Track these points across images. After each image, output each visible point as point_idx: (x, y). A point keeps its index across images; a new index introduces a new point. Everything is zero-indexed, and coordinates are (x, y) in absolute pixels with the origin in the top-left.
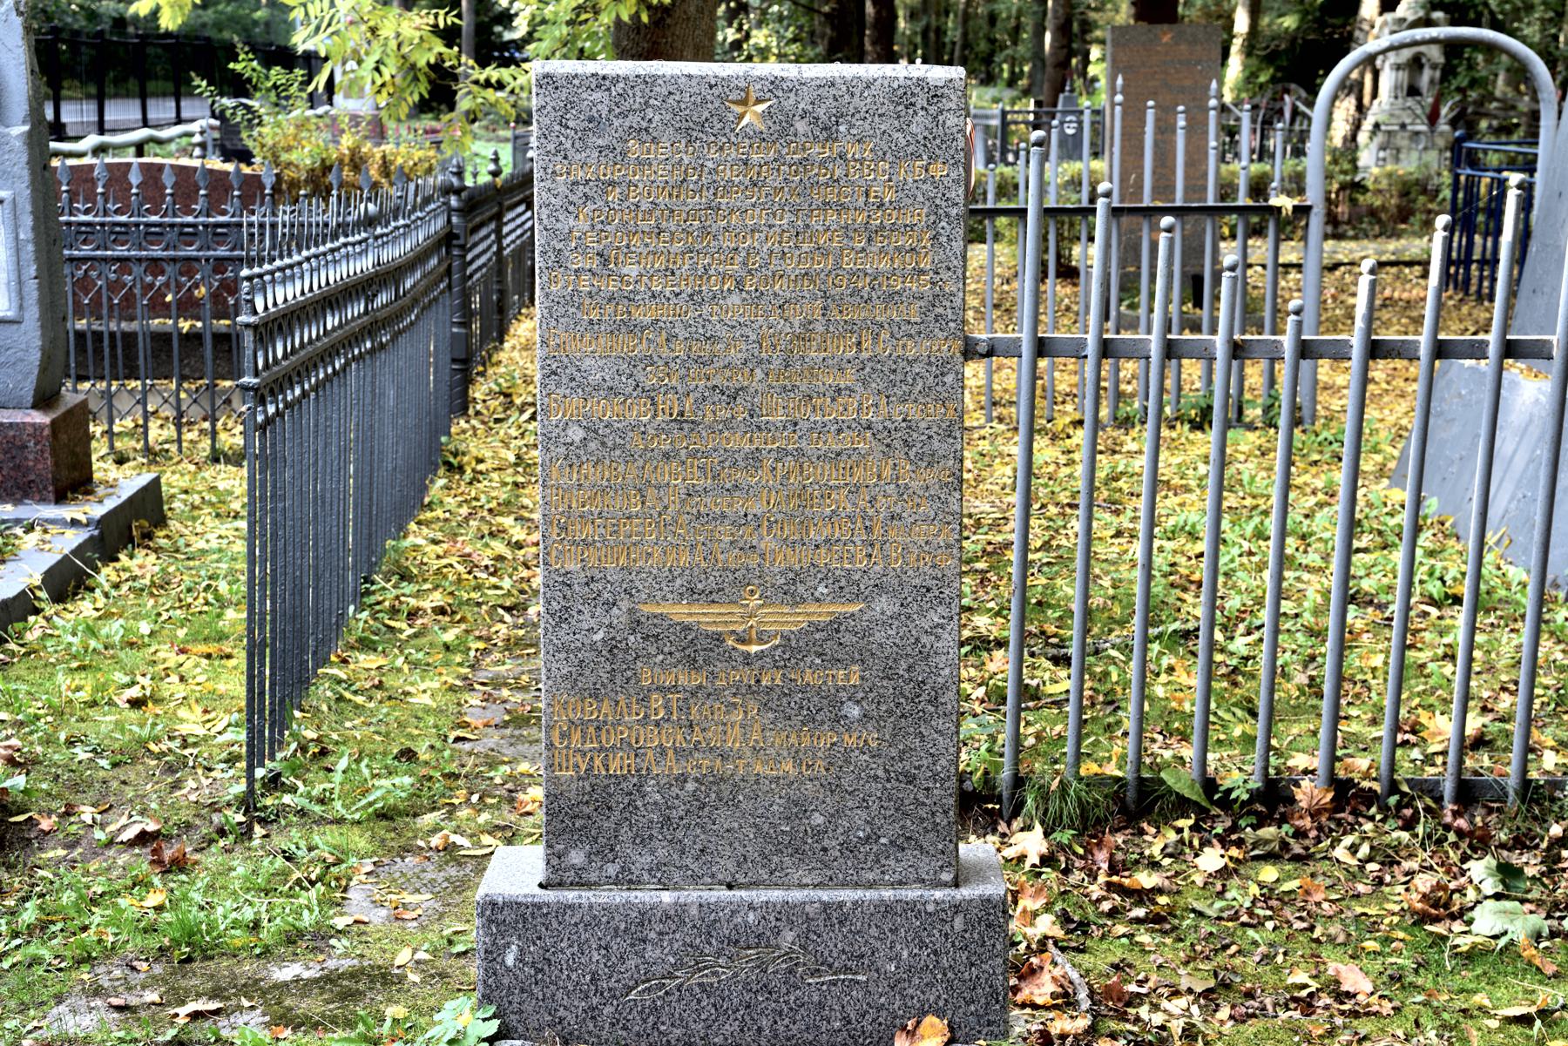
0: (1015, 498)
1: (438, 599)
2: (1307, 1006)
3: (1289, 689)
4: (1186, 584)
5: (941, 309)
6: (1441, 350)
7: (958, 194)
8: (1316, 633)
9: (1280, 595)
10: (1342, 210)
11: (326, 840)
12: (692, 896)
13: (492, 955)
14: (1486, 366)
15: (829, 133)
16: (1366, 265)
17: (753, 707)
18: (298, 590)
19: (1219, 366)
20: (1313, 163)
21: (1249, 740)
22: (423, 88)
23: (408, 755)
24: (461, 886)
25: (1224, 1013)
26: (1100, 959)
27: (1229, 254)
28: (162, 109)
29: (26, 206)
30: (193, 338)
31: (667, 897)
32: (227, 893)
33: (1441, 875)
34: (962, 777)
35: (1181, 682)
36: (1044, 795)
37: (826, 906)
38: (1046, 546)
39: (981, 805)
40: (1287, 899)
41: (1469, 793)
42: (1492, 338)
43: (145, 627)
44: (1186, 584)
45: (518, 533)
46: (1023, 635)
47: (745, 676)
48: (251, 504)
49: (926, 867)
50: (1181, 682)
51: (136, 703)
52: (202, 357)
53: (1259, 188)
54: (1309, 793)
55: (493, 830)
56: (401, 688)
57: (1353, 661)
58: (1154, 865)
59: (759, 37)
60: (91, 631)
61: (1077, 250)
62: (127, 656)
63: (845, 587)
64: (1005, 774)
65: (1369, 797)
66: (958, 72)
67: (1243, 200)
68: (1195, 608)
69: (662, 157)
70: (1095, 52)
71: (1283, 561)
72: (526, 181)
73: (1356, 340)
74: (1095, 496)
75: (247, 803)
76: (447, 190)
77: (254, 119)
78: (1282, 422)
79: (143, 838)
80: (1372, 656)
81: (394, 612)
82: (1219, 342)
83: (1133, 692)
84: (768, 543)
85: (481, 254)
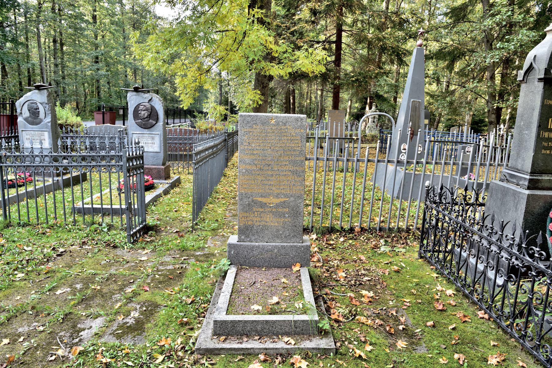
0: (313, 182)
1: (222, 196)
2: (356, 262)
3: (354, 213)
4: (340, 196)
5: (302, 152)
6: (378, 161)
7: (305, 135)
8: (358, 204)
9: (353, 198)
10: (364, 139)
11: (204, 233)
12: (261, 244)
13: (230, 252)
14: (385, 164)
15: (285, 124)
16: (368, 147)
17: (271, 214)
18: (201, 194)
19: (345, 162)
20: (359, 132)
21: (348, 221)
22: (223, 117)
23: (217, 220)
24: (225, 241)
25: (343, 263)
26: (324, 254)
27: (347, 145)
28: (183, 120)
29: (162, 135)
30: (186, 155)
31: (257, 244)
32: (189, 241)
33: (376, 242)
34: (304, 226)
35: (338, 212)
36: (316, 229)
37: (282, 246)
38: (317, 190)
39: (306, 230)
40: (353, 245)
41: (381, 229)
42: (386, 159)
43: (177, 200)
44: (340, 196)
45: (235, 186)
46: (314, 204)
47: (270, 210)
48: (194, 181)
49: (298, 240)
50: (338, 212)
51: (176, 211)
52: (186, 158)
53: (351, 135)
54: (357, 229)
55: (230, 232)
56: (217, 209)
57: (364, 209)
58: (333, 240)
59: (274, 110)
60: (170, 200)
61: (323, 144)
62: (175, 204)
63: (286, 196)
64: (310, 226)
65: (366, 230)
66: (305, 116)
67: (349, 137)
68: (341, 200)
69: (258, 128)
70: (326, 114)
71: (354, 193)
72: (237, 131)
73: (366, 159)
74: (326, 182)
75: (192, 227)
76: (225, 133)
77: (196, 122)
78: (354, 172)
79: (177, 232)
80: (367, 208)
81: (215, 198)
82: (345, 158)
83: (331, 213)
84: (274, 189)
85: (230, 143)
